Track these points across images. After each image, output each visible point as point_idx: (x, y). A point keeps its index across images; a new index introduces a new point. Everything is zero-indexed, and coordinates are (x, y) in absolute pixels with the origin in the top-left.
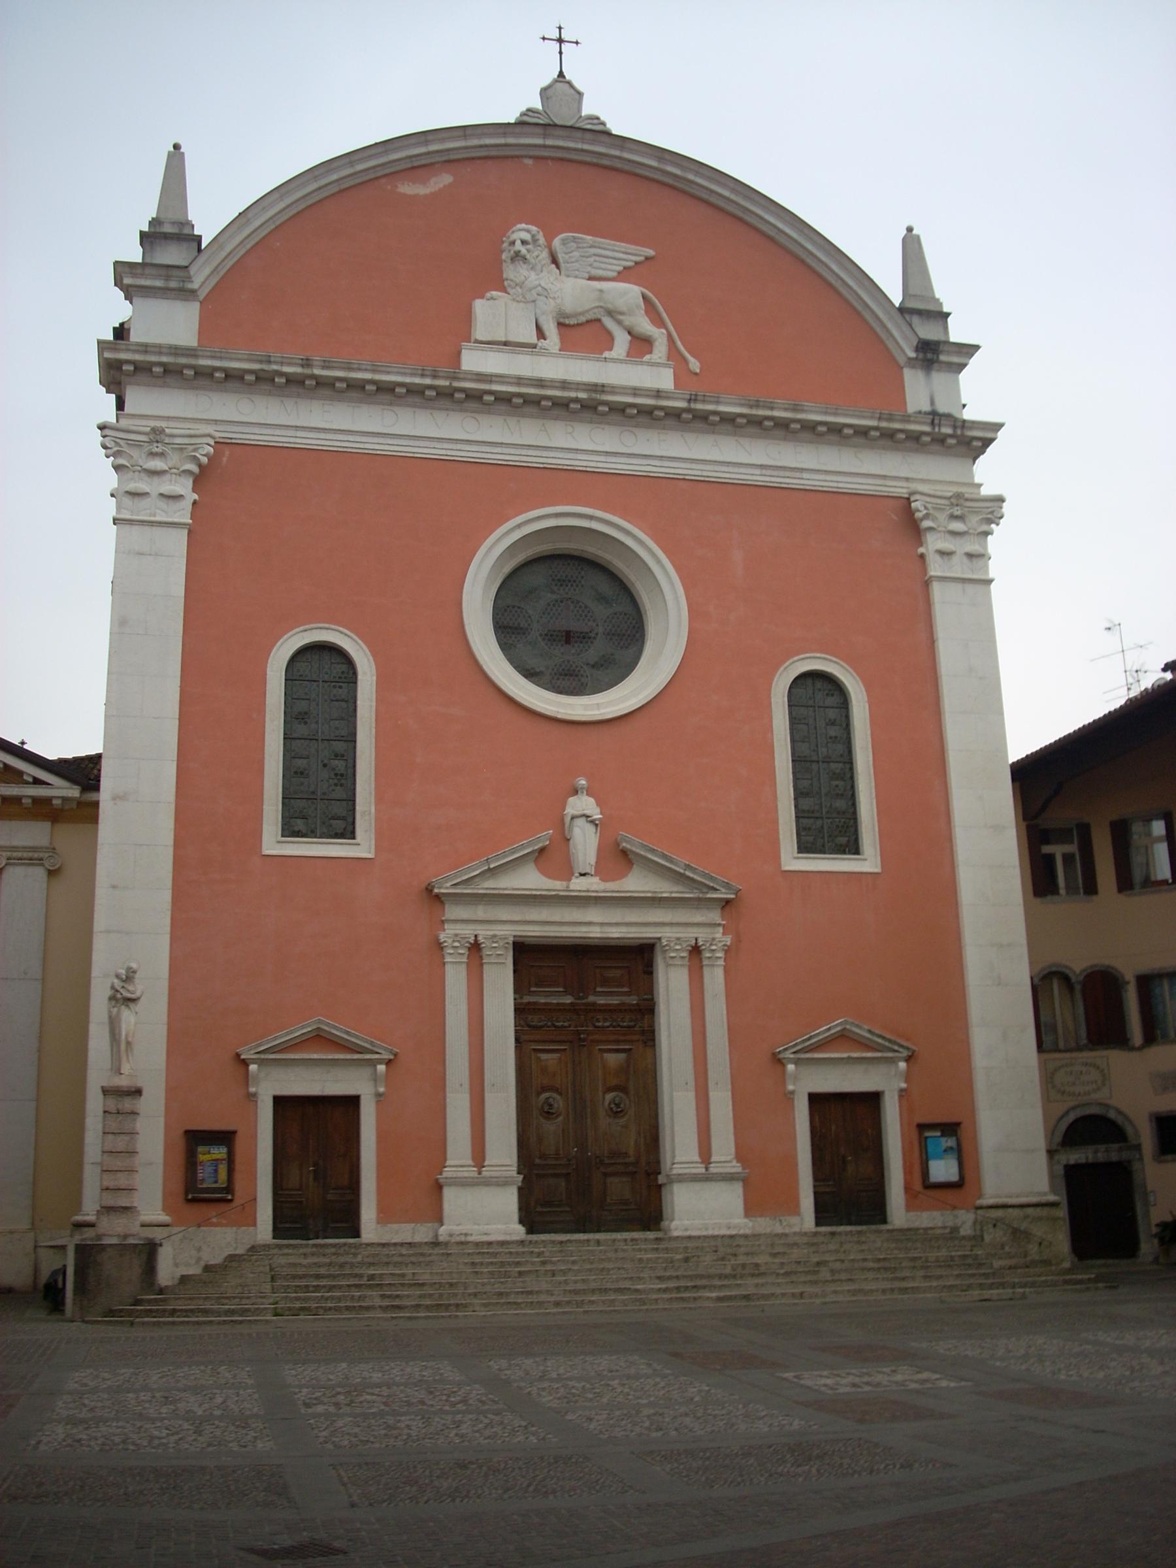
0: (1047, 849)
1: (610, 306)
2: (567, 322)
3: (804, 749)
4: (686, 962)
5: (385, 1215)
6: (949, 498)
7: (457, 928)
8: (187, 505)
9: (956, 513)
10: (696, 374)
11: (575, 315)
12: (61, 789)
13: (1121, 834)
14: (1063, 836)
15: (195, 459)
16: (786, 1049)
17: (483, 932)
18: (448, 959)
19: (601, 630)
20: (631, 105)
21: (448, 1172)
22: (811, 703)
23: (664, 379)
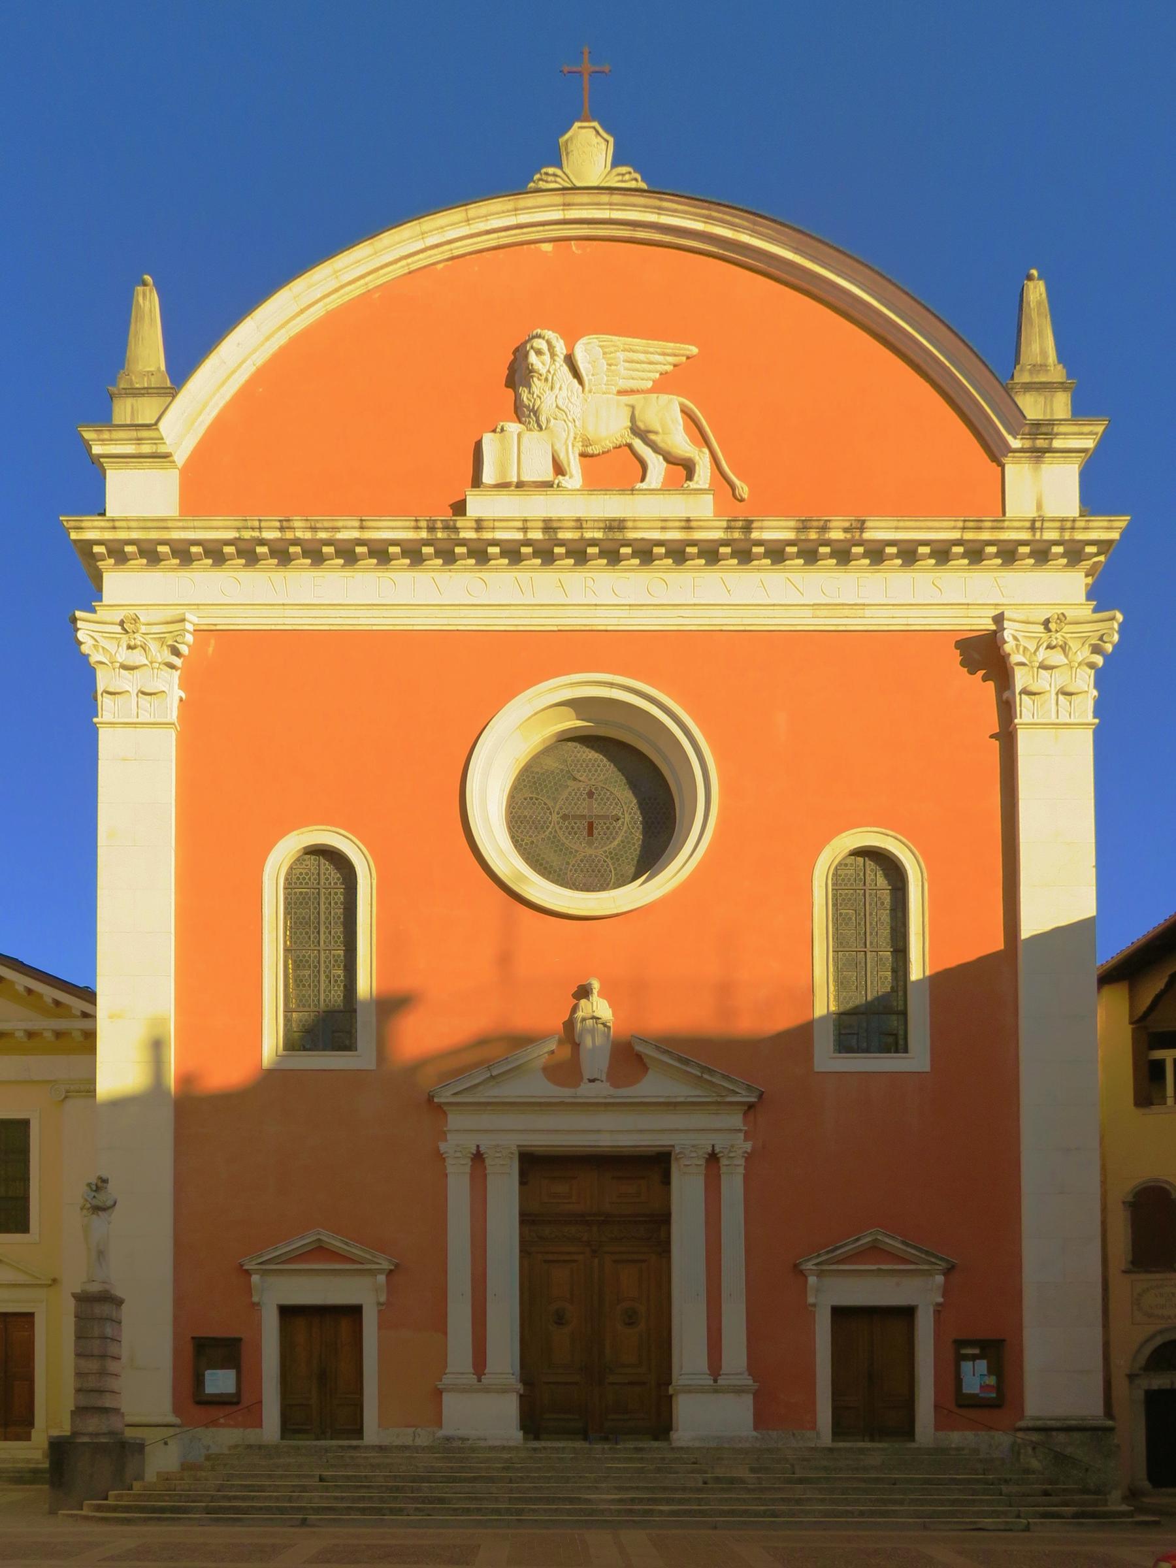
0: (1158, 1054)
2: (590, 450)
4: (702, 1169)
7: (461, 1134)
10: (742, 500)
16: (808, 1260)
17: (486, 1142)
18: (450, 1170)
21: (447, 1380)
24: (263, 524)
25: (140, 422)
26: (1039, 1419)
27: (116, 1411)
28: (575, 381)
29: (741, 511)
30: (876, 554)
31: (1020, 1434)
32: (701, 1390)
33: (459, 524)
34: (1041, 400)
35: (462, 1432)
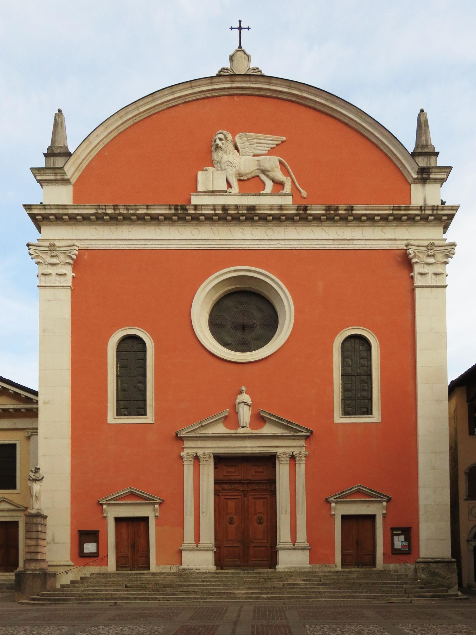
1: (263, 168)
2: (242, 178)
3: (349, 370)
4: (288, 462)
5: (158, 564)
6: (427, 246)
9: (430, 254)
10: (305, 198)
11: (246, 175)
15: (70, 257)
16: (332, 497)
17: (200, 452)
18: (185, 463)
19: (258, 323)
20: (277, 60)
21: (184, 546)
22: (353, 349)
23: (288, 201)
24: (107, 207)
25: (57, 166)
26: (424, 558)
27: (44, 560)
28: (236, 151)
29: (303, 203)
30: (358, 219)
31: (417, 565)
32: (288, 549)
33: (187, 207)
34: (425, 159)
35: (190, 567)
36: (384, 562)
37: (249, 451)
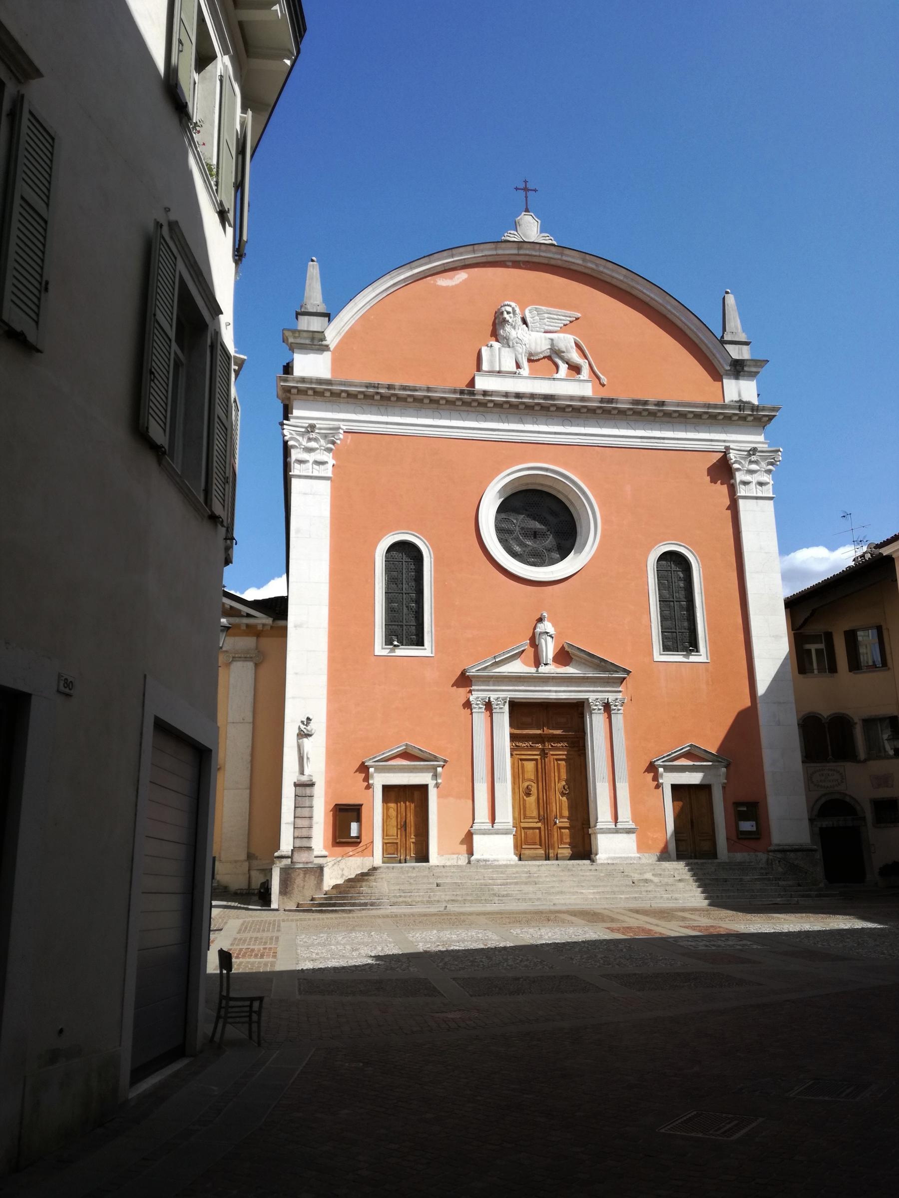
0: (807, 646)
5: (440, 853)
8: (330, 466)
10: (603, 385)
11: (537, 354)
12: (262, 619)
13: (851, 638)
14: (815, 639)
17: (493, 696)
26: (779, 845)
35: (485, 857)
36: (729, 851)
37: (553, 696)
